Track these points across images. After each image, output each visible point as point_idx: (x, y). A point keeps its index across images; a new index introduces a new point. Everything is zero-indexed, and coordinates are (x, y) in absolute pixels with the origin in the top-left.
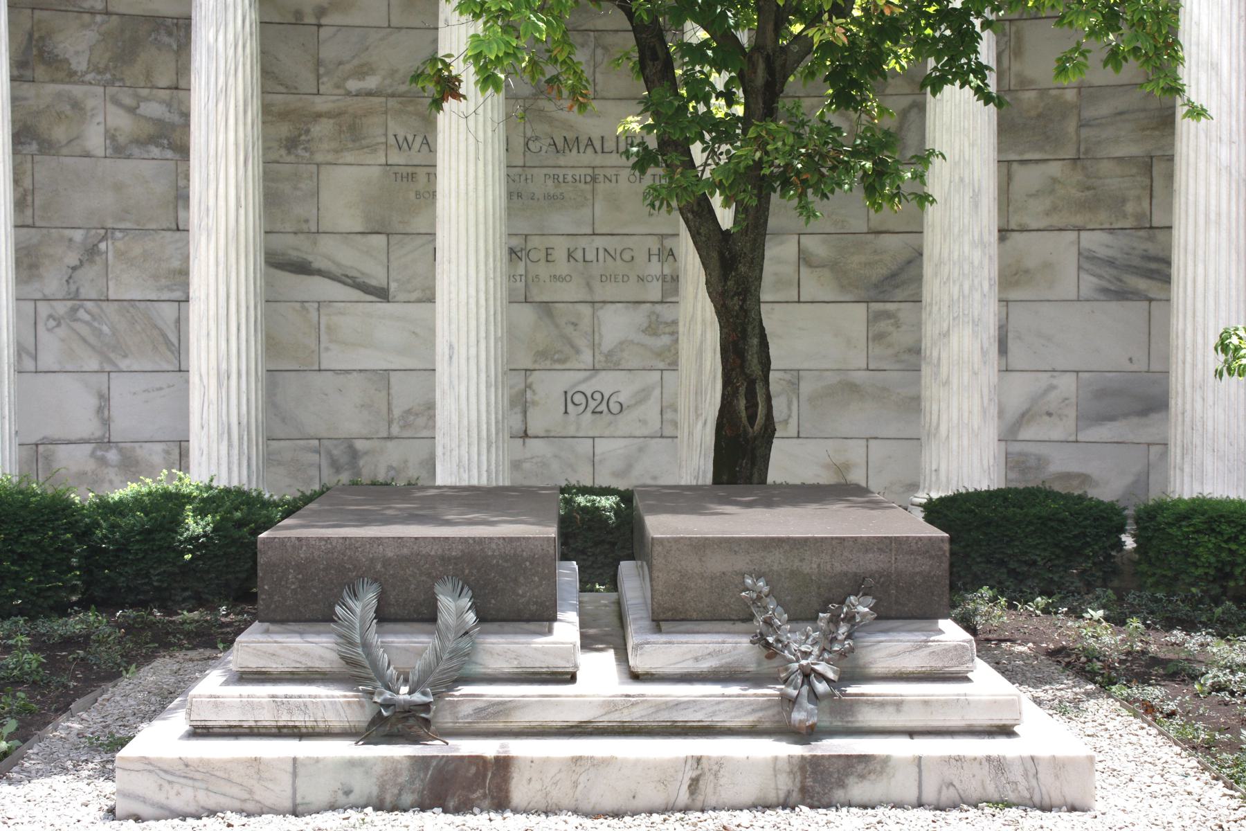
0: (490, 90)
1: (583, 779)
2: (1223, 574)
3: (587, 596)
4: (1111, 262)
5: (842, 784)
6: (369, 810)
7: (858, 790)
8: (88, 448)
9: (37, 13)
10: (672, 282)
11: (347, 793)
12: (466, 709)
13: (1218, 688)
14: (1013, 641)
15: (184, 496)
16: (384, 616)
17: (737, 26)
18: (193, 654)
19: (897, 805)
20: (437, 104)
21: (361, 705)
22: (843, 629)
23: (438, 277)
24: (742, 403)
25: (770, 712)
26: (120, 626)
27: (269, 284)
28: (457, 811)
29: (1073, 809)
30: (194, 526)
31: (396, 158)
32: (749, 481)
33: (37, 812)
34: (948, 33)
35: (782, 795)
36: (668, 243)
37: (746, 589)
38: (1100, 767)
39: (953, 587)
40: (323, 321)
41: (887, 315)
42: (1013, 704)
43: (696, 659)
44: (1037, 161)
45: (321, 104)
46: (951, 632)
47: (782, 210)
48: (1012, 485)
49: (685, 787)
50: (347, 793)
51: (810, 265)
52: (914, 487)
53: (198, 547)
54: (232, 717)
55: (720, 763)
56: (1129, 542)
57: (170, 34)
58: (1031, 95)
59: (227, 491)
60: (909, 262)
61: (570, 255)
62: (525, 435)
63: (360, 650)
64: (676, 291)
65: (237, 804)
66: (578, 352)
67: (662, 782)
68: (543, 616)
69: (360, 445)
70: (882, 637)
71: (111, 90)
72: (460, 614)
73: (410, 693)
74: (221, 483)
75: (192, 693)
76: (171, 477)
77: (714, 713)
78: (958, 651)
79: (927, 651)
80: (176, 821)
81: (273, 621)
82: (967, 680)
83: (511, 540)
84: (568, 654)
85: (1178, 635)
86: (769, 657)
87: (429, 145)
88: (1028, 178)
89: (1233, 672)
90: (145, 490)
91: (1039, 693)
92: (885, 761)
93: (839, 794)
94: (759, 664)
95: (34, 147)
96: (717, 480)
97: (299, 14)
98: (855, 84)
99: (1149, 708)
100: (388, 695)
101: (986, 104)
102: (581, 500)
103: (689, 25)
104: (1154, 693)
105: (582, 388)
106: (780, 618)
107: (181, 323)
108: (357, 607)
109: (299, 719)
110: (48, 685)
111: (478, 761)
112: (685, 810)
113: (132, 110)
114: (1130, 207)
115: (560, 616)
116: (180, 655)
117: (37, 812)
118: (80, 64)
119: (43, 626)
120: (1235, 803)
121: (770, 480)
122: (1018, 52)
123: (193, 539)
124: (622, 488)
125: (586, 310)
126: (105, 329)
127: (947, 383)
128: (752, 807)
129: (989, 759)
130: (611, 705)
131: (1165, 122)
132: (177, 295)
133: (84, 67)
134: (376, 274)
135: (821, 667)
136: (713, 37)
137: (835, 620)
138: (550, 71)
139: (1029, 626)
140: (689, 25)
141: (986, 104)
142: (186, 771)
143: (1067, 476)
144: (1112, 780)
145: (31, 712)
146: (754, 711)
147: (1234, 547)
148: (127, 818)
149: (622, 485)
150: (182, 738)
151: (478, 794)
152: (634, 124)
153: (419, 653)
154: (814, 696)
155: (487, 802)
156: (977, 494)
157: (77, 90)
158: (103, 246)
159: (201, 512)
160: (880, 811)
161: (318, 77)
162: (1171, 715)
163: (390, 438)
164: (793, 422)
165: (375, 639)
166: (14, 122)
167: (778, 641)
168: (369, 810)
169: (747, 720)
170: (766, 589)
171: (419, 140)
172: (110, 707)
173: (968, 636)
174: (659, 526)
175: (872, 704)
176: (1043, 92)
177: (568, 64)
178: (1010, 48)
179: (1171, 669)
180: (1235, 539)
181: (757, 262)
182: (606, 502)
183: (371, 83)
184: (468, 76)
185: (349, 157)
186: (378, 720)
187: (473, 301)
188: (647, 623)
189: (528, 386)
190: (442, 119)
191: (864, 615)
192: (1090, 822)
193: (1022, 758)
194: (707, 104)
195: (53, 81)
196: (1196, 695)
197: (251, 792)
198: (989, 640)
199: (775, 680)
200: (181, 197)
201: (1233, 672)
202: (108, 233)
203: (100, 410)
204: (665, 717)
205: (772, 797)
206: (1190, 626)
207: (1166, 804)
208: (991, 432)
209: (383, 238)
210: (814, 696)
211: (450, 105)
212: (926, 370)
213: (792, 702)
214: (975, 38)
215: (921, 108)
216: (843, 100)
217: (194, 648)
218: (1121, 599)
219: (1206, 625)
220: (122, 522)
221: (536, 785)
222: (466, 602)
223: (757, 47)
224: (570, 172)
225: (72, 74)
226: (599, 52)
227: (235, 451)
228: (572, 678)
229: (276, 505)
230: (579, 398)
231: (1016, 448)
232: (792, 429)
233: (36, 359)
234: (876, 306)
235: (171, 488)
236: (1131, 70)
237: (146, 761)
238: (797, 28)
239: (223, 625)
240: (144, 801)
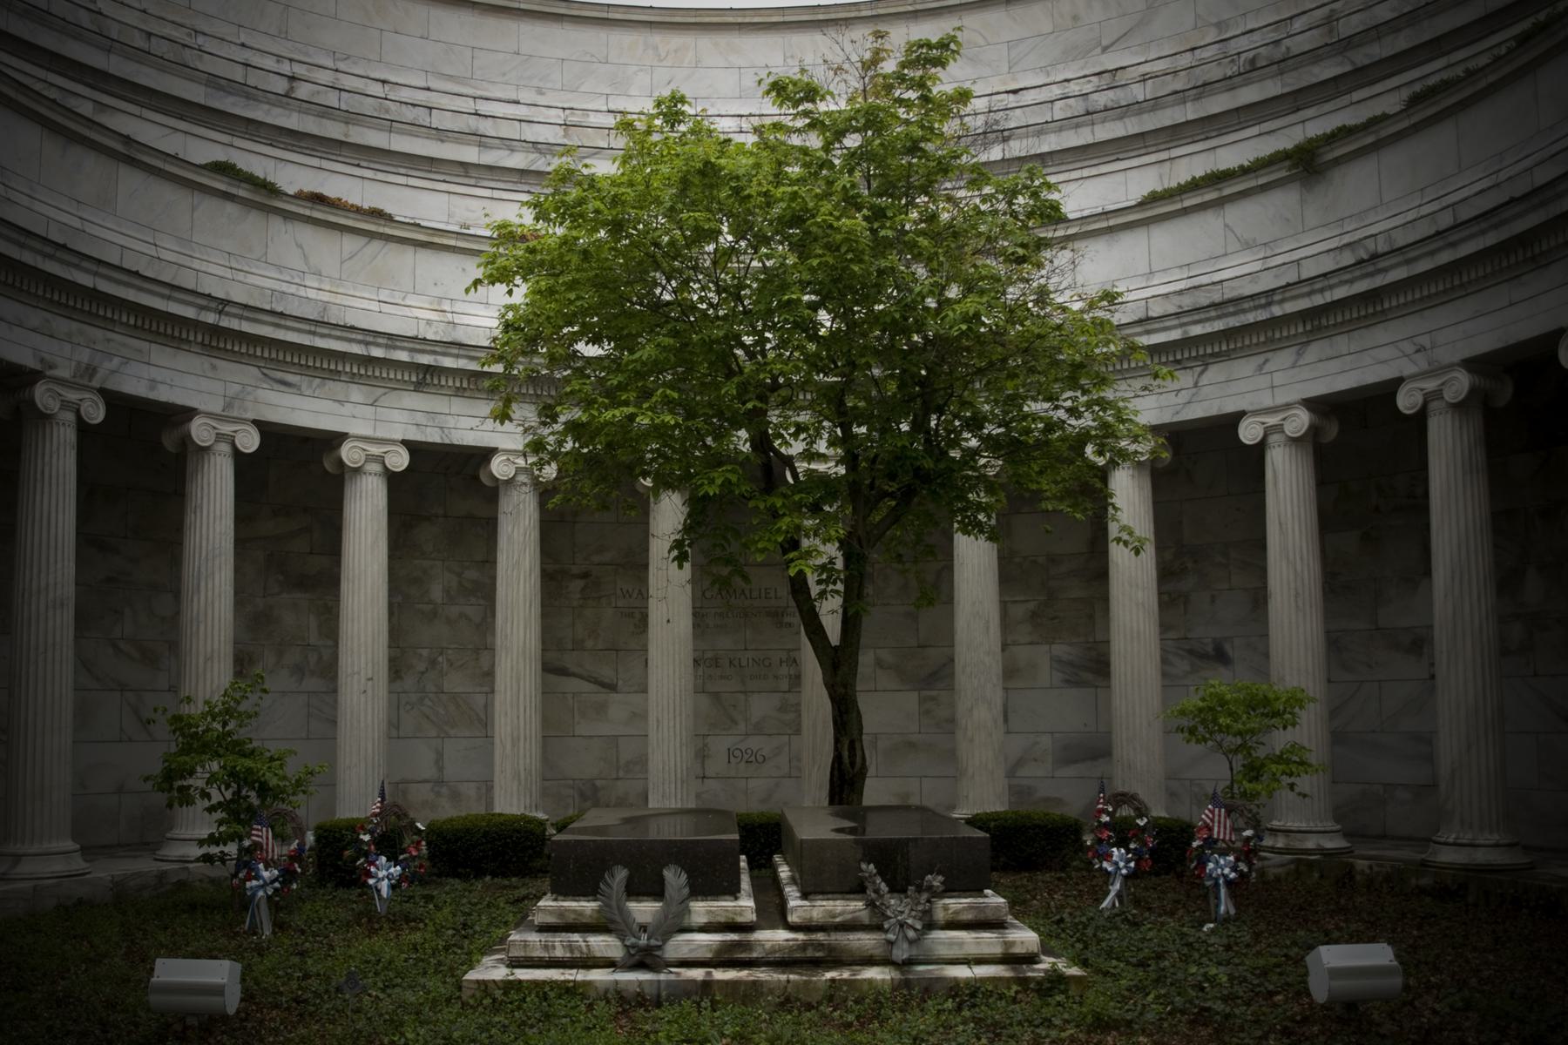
27: (544, 683)
125: (742, 697)
203: (437, 762)
230: (737, 753)
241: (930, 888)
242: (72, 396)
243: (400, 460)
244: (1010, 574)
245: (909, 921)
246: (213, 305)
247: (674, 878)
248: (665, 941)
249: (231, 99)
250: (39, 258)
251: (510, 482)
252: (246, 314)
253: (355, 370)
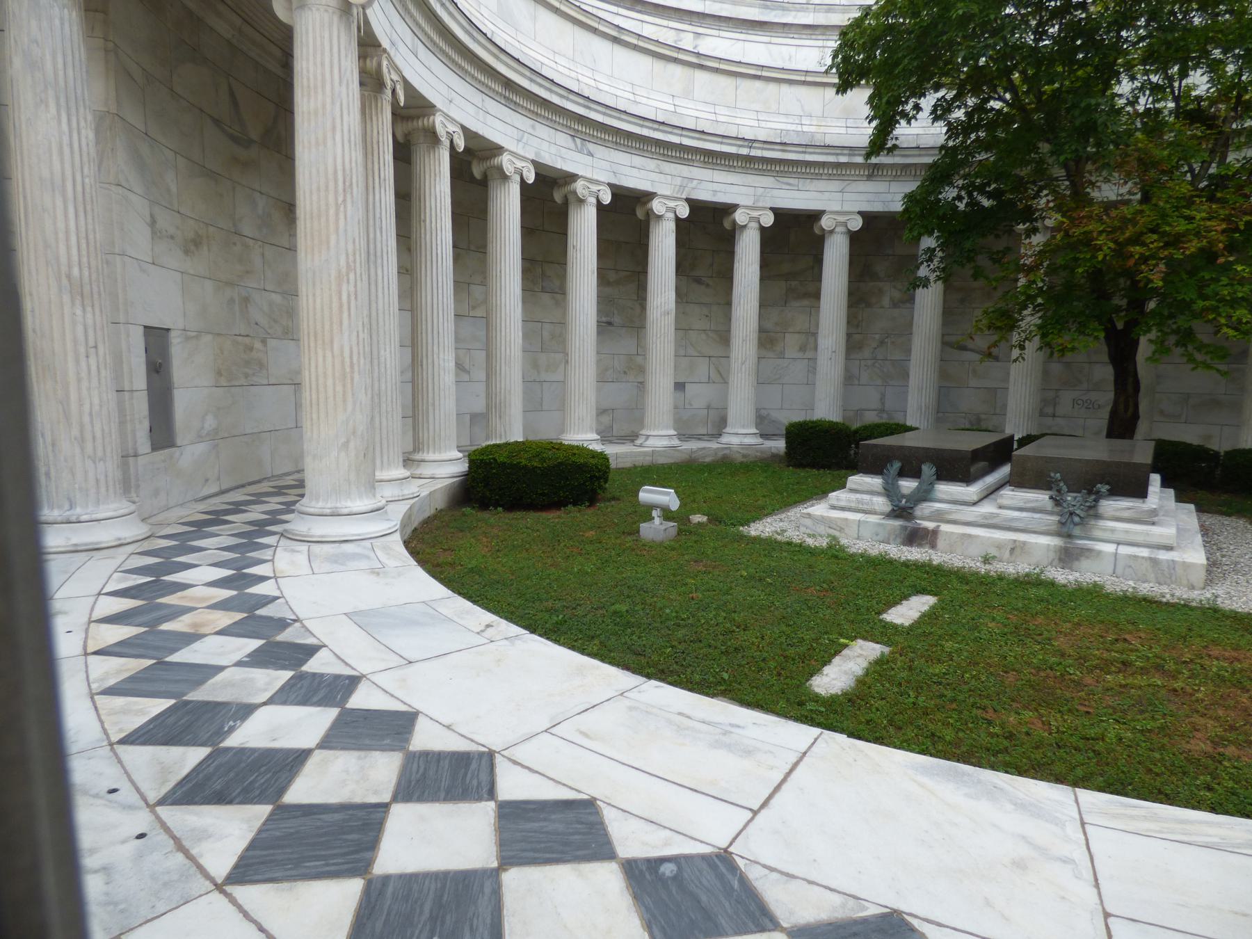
8: (875, 413)
27: (942, 351)
69: (983, 416)
73: (906, 502)
94: (1053, 508)
106: (1065, 488)
146: (1046, 526)
188: (401, 464)
203: (881, 399)
230: (1079, 402)
241: (1098, 492)
242: (672, 204)
243: (768, 220)
244: (949, 314)
245: (1077, 512)
246: (746, 144)
247: (928, 470)
248: (916, 505)
249: (774, 13)
250: (651, 131)
251: (832, 232)
252: (766, 146)
253: (830, 172)
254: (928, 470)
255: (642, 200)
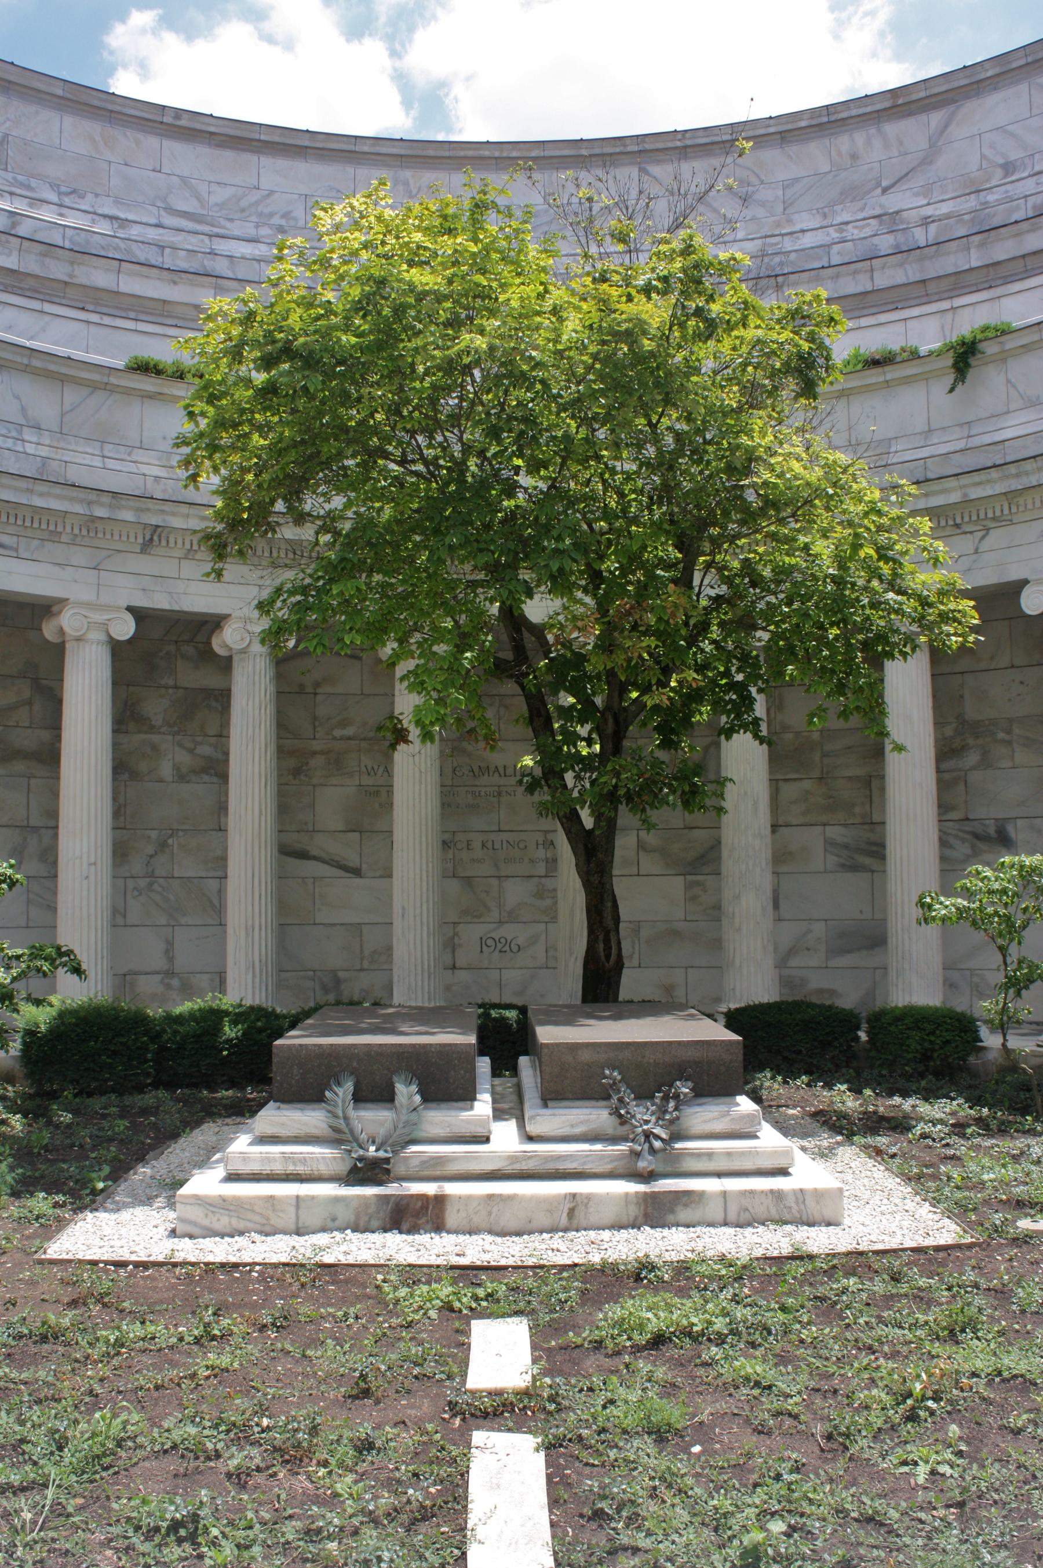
0: (429, 744)
1: (495, 1210)
2: (926, 1057)
3: (497, 1081)
4: (846, 847)
5: (672, 1211)
6: (348, 1231)
7: (683, 1215)
8: (158, 977)
9: (131, 688)
10: (552, 863)
11: (334, 1220)
12: (414, 1162)
13: (924, 1136)
14: (787, 1106)
15: (223, 1011)
16: (360, 1098)
17: (594, 694)
18: (228, 1120)
19: (711, 1225)
20: (393, 747)
21: (342, 1159)
22: (672, 1104)
23: (395, 861)
24: (601, 947)
25: (623, 1162)
26: (179, 1100)
28: (409, 1232)
29: (829, 1224)
30: (230, 1031)
31: (367, 781)
32: (606, 1000)
33: (123, 1231)
34: (734, 697)
35: (631, 1219)
36: (550, 836)
37: (605, 1077)
38: (846, 1194)
39: (745, 1068)
40: (317, 890)
41: (698, 884)
42: (788, 1153)
43: (572, 1126)
44: (795, 780)
45: (317, 745)
46: (745, 1104)
47: (625, 816)
48: (784, 999)
49: (565, 1214)
50: (334, 1220)
51: (645, 850)
52: (718, 1000)
53: (232, 1046)
54: (255, 1167)
55: (589, 1198)
56: (863, 1036)
57: (217, 700)
58: (790, 736)
59: (252, 1008)
60: (712, 848)
61: (483, 845)
62: (454, 967)
63: (342, 1121)
64: (555, 869)
65: (259, 1227)
66: (489, 910)
67: (550, 1211)
68: (468, 1096)
69: (342, 975)
70: (697, 1109)
71: (178, 738)
72: (410, 1097)
73: (377, 1150)
74: (248, 1002)
75: (229, 1150)
76: (214, 998)
77: (584, 1163)
78: (750, 1117)
79: (728, 1118)
80: (217, 1239)
81: (283, 1101)
82: (757, 1137)
83: (445, 1045)
84: (484, 1123)
85: (897, 1100)
86: (622, 1124)
87: (388, 772)
88: (790, 791)
89: (934, 1125)
90: (196, 1007)
91: (805, 1143)
92: (701, 1194)
93: (671, 1218)
94: (615, 1129)
95: (127, 776)
96: (585, 1000)
97: (302, 686)
98: (673, 731)
99: (879, 1152)
100: (361, 1152)
101: (761, 743)
102: (494, 1014)
103: (562, 694)
104: (882, 1141)
105: (493, 935)
107: (221, 893)
108: (340, 1091)
109: (300, 1169)
110: (130, 1141)
111: (423, 1198)
112: (565, 1230)
113: (191, 751)
114: (857, 810)
115: (478, 1096)
116: (220, 1121)
117: (123, 1231)
118: (157, 721)
119: (128, 1100)
120: (937, 1217)
121: (620, 999)
122: (780, 708)
123: (229, 1041)
124: (520, 1004)
125: (495, 882)
126: (172, 897)
127: (739, 930)
128: (611, 1227)
129: (772, 1191)
130: (513, 1158)
131: (878, 753)
132: (219, 874)
133: (159, 722)
134: (352, 859)
135: (657, 1131)
136: (579, 702)
137: (666, 1098)
138: (470, 724)
139: (797, 1096)
140: (562, 694)
141: (761, 743)
142: (223, 1204)
143: (821, 991)
144: (855, 1203)
145: (120, 1161)
147: (932, 1038)
148: (183, 1236)
149: (520, 1002)
150: (222, 1181)
151: (423, 1220)
152: (528, 761)
153: (382, 1124)
154: (653, 1151)
155: (429, 1226)
156: (761, 1005)
157: (155, 738)
158: (170, 841)
159: (234, 1022)
160: (698, 1229)
161: (315, 728)
162: (893, 1156)
163: (362, 970)
164: (636, 956)
165: (352, 1113)
166: (114, 759)
167: (628, 1113)
168: (348, 1231)
169: (607, 1167)
170: (619, 1077)
171: (381, 769)
172: (172, 1158)
173: (756, 1107)
174: (546, 1034)
175: (693, 1155)
176: (798, 734)
177: (483, 720)
178: (775, 706)
179: (893, 1123)
180: (932, 1033)
181: (610, 851)
182: (512, 1014)
183: (350, 731)
184: (414, 733)
185: (335, 780)
186: (354, 1170)
187: (418, 877)
188: (538, 1101)
189: (456, 934)
190: (397, 756)
191: (685, 1094)
192: (841, 1233)
193: (794, 1191)
194: (575, 746)
195: (140, 732)
196: (910, 1142)
197: (268, 1219)
198: (771, 1106)
199: (625, 1139)
200: (222, 808)
201: (934, 1125)
202: (174, 833)
203: (167, 951)
204: (551, 1166)
205: (624, 1220)
206: (905, 1094)
207: (891, 1219)
208: (769, 963)
209: (357, 834)
210: (653, 1151)
211: (402, 747)
212: (725, 921)
213: (637, 1155)
214: (752, 701)
215: (718, 745)
216: (668, 744)
217: (229, 1116)
218: (859, 1075)
219: (915, 1093)
220: (181, 1029)
221: (463, 1214)
222: (414, 1088)
223: (608, 708)
224: (483, 790)
225: (152, 727)
226: (502, 710)
227: (257, 980)
228: (487, 1140)
229: (285, 1017)
230: (490, 942)
231: (786, 972)
232: (635, 962)
233: (125, 916)
234: (690, 878)
235: (215, 1006)
236: (855, 720)
237: (195, 1197)
238: (634, 695)
239: (249, 1100)
240: (195, 1224)
247: (406, 1092)
254: (406, 1092)
255: (55, 609)
